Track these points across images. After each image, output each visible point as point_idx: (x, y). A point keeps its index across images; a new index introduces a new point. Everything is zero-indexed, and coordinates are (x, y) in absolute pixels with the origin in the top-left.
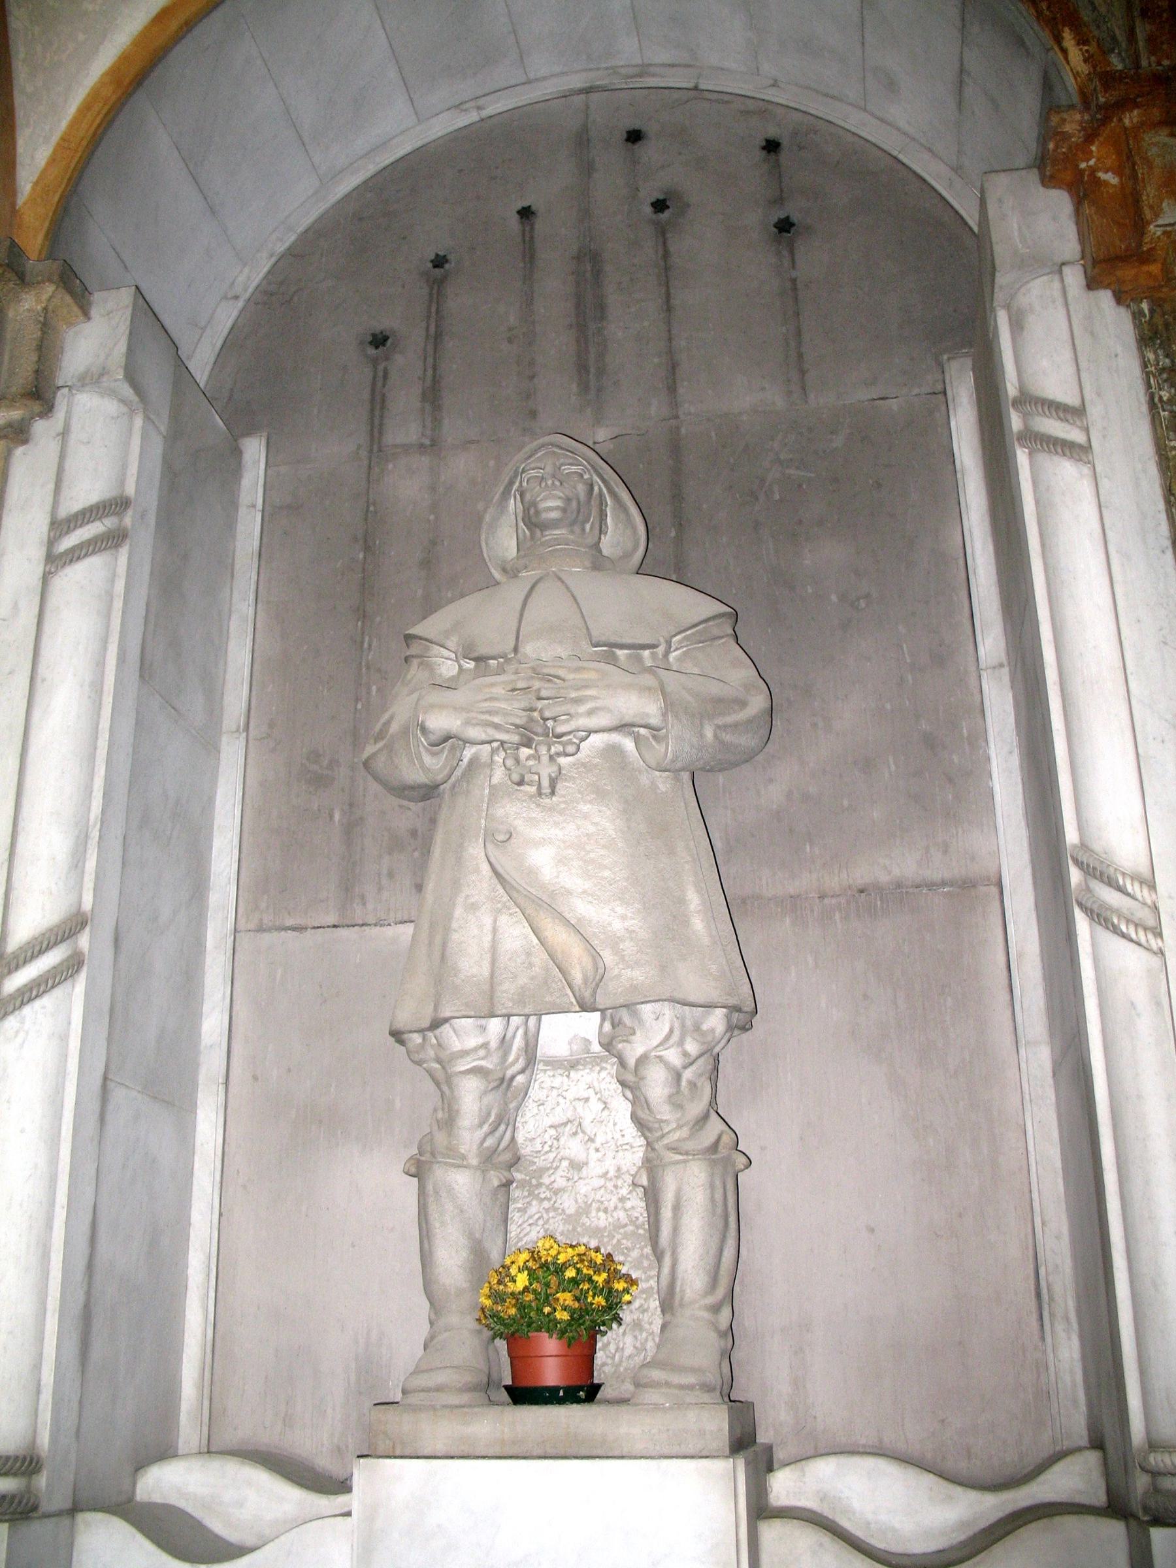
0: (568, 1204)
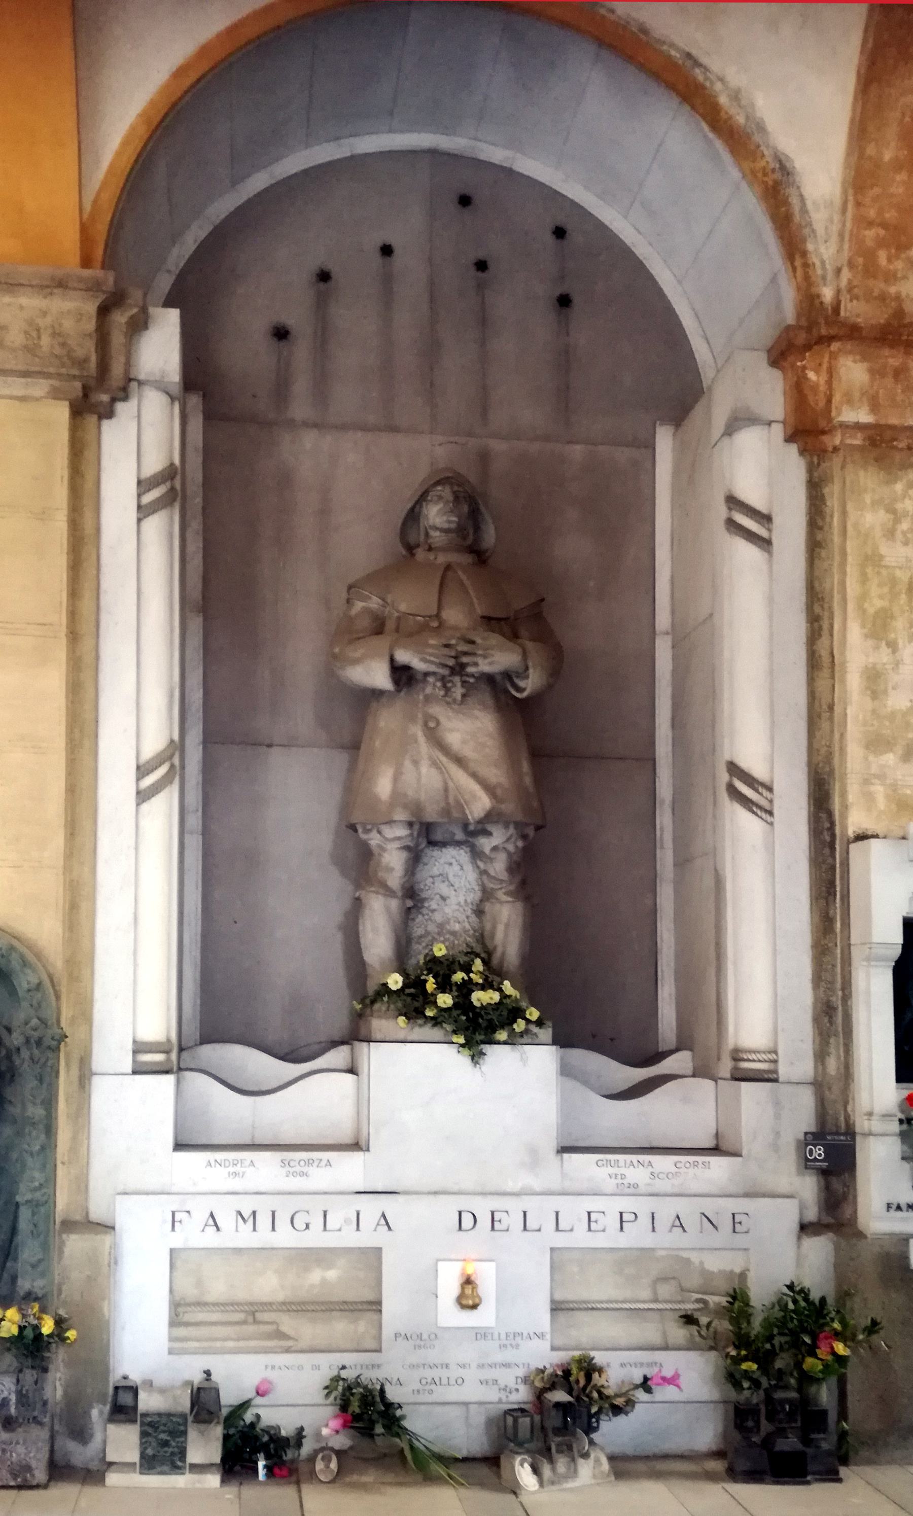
0: (438, 917)
